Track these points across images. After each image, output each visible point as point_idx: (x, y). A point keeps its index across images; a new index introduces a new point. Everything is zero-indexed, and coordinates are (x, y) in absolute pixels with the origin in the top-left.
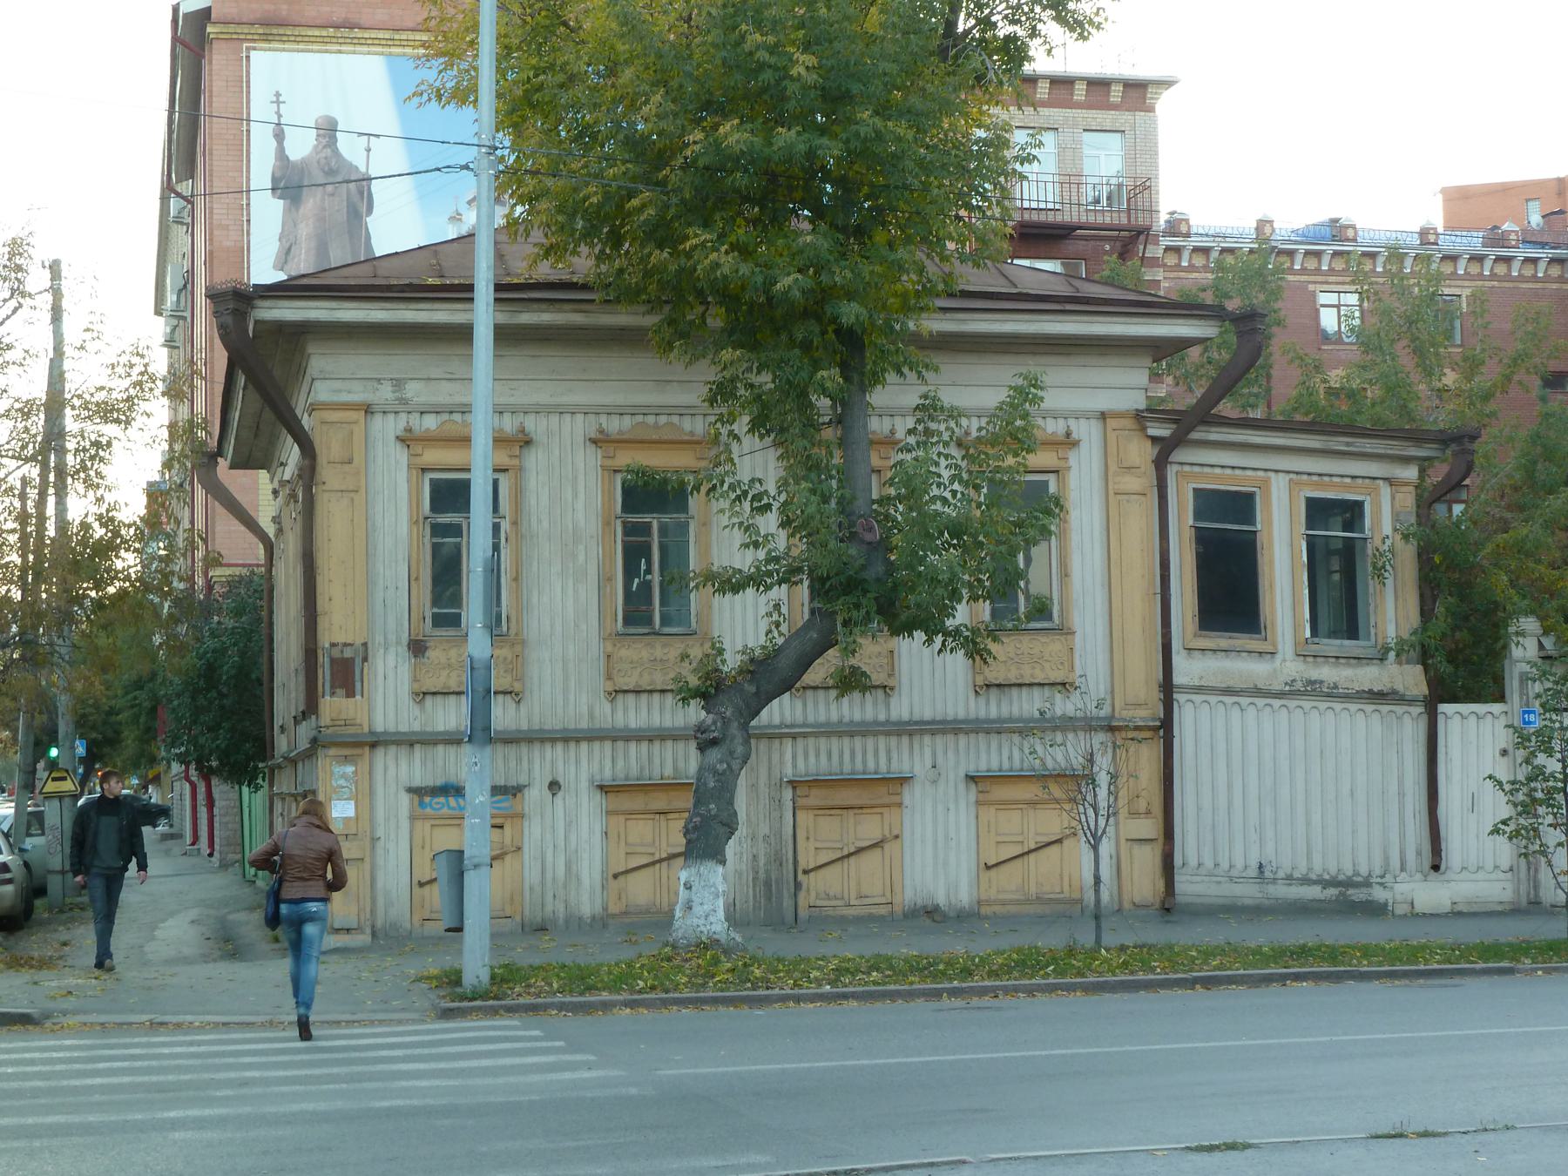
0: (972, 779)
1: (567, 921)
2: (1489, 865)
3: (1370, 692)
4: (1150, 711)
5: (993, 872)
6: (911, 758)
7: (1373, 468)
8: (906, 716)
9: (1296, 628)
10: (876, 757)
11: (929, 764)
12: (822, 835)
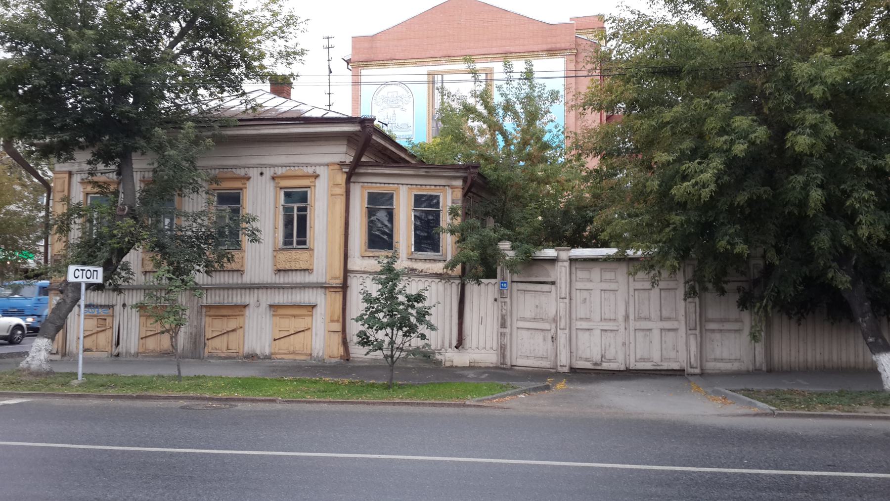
0: (270, 306)
1: (126, 353)
2: (488, 347)
3: (436, 274)
4: (338, 282)
5: (467, 342)
6: (248, 298)
7: (442, 182)
8: (248, 282)
9: (409, 247)
10: (237, 298)
11: (256, 299)
12: (213, 326)
